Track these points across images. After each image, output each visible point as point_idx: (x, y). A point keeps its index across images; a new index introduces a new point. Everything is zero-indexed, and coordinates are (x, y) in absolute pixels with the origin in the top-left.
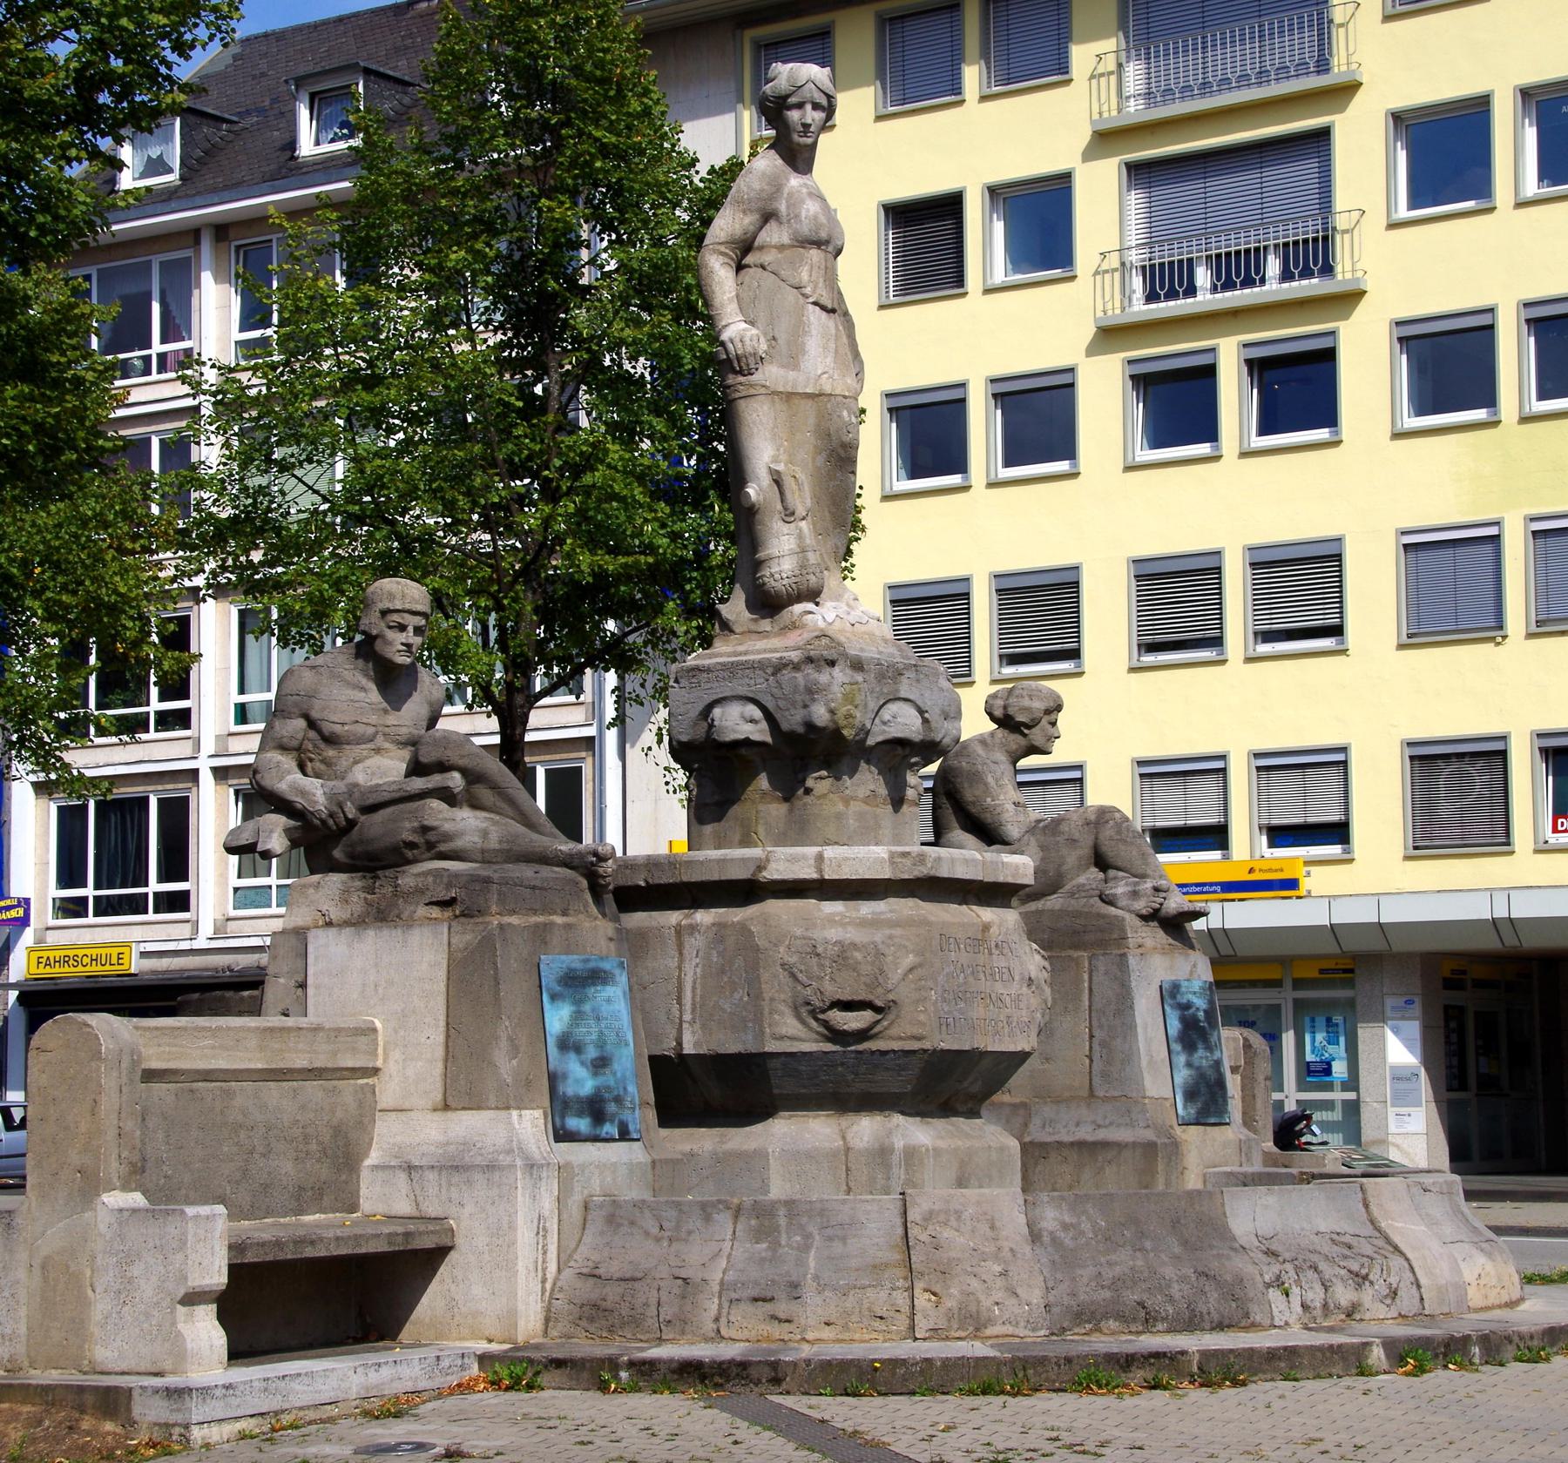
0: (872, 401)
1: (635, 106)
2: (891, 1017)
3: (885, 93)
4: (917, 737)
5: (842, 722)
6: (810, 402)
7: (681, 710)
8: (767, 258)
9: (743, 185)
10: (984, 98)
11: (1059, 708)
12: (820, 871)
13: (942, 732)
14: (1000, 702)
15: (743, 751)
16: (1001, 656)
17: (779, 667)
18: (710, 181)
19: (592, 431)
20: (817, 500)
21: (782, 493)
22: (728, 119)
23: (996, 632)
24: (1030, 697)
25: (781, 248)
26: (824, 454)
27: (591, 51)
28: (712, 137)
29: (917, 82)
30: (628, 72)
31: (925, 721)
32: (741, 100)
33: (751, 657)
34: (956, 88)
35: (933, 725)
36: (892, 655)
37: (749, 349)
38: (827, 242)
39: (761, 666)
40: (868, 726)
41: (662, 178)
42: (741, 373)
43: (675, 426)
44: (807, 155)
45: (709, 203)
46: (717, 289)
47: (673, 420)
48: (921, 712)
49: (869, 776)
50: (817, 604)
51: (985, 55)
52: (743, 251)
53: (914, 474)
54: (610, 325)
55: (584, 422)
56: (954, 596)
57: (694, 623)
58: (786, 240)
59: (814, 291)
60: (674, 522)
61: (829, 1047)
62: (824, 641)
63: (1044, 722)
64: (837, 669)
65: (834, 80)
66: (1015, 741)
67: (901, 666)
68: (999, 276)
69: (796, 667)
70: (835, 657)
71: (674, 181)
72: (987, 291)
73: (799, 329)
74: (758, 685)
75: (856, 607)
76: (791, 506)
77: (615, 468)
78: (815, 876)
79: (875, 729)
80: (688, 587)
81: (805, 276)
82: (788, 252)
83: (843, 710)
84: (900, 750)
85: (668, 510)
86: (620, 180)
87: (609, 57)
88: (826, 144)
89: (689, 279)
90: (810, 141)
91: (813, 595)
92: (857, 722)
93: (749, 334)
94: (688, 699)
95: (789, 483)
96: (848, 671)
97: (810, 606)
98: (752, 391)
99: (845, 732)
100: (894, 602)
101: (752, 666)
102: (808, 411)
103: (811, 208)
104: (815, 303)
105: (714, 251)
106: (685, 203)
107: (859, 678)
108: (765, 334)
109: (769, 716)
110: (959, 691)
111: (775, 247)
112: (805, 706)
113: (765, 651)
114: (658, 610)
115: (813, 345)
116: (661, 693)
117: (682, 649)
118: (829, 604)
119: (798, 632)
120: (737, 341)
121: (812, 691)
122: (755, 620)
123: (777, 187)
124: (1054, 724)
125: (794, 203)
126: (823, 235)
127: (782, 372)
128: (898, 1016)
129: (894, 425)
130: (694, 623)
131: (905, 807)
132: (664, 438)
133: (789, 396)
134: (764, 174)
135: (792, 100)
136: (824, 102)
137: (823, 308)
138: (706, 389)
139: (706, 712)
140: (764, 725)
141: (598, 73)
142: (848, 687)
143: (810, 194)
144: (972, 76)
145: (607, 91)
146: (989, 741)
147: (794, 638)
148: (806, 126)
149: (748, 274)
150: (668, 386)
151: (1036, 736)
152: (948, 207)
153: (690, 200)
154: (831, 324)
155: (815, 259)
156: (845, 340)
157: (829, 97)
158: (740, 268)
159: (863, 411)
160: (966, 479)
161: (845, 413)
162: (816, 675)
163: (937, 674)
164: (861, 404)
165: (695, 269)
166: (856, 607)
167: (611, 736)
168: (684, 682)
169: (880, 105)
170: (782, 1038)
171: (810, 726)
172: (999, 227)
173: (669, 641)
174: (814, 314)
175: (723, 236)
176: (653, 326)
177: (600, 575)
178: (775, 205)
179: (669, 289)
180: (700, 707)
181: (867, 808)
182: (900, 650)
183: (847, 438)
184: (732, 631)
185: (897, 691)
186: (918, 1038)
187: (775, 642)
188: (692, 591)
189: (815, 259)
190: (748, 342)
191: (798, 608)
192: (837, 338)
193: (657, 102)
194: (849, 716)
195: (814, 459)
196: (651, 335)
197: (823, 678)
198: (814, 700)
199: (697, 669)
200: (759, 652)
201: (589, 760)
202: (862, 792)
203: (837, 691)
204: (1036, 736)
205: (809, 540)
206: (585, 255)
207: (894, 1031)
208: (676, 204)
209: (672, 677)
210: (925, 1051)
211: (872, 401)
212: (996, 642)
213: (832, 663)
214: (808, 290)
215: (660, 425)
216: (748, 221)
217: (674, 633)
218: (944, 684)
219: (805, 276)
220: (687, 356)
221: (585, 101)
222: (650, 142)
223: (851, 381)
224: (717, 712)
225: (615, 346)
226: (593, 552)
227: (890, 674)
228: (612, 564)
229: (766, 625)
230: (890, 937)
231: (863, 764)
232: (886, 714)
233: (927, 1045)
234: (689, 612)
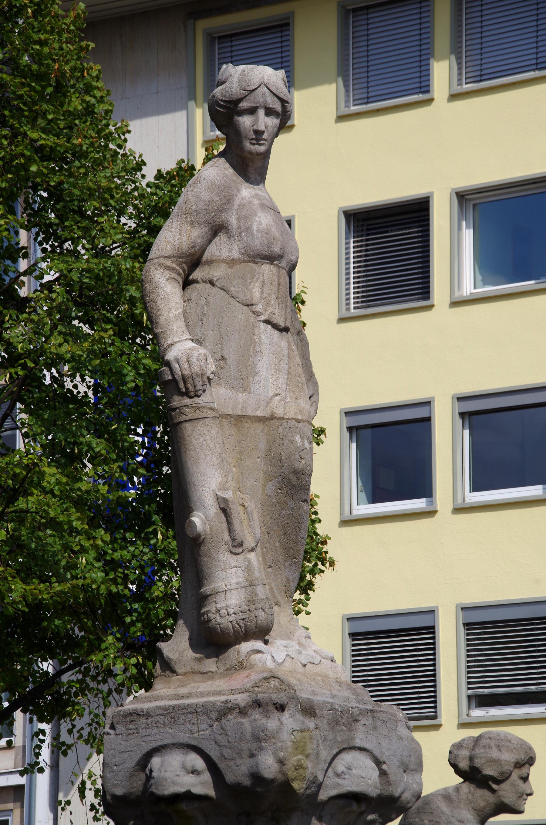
0: (329, 417)
1: (76, 104)
3: (347, 91)
4: (373, 792)
5: (292, 774)
6: (260, 427)
7: (118, 759)
8: (217, 272)
9: (192, 195)
10: (454, 97)
11: (531, 761)
13: (402, 785)
14: (465, 753)
15: (183, 806)
16: (469, 697)
17: (225, 711)
18: (157, 186)
19: (28, 453)
20: (267, 530)
21: (229, 523)
22: (180, 116)
23: (464, 670)
24: (499, 748)
25: (231, 262)
26: (275, 482)
27: (28, 41)
28: (162, 137)
29: (383, 79)
30: (67, 68)
31: (383, 774)
32: (192, 96)
33: (194, 701)
34: (424, 87)
35: (392, 777)
36: (348, 699)
37: (196, 369)
38: (280, 257)
39: (204, 710)
40: (320, 778)
41: (104, 183)
42: (187, 394)
43: (116, 447)
44: (259, 164)
45: (156, 212)
46: (162, 305)
47: (113, 440)
48: (378, 763)
50: (266, 642)
51: (456, 50)
52: (191, 264)
53: (374, 499)
54: (47, 338)
55: (20, 444)
56: (419, 632)
57: (133, 661)
58: (236, 255)
59: (266, 309)
60: (114, 550)
62: (273, 683)
63: (515, 776)
64: (287, 714)
65: (290, 83)
66: (483, 797)
67: (356, 711)
68: (468, 288)
69: (243, 712)
70: (284, 700)
71: (117, 188)
72: (455, 304)
73: (250, 348)
74: (202, 732)
75: (311, 645)
76: (239, 537)
77: (52, 492)
79: (328, 782)
80: (128, 620)
81: (256, 292)
82: (238, 267)
83: (293, 761)
84: (355, 806)
85: (108, 538)
86: (61, 183)
87: (46, 50)
88: (282, 150)
89: (133, 291)
90: (262, 149)
91: (262, 633)
92: (308, 774)
93: (196, 354)
94: (125, 747)
95: (236, 511)
96: (299, 717)
97: (258, 644)
98: (199, 414)
99: (295, 785)
100: (353, 635)
101: (195, 711)
102: (258, 435)
103: (263, 220)
104: (267, 322)
105: (160, 265)
106: (130, 209)
107: (311, 724)
108: (213, 354)
109: (212, 766)
110: (418, 736)
111: (225, 262)
112: (252, 756)
113: (209, 694)
114: (95, 646)
115: (264, 365)
116: (95, 741)
117: (119, 692)
118: (279, 643)
119: (245, 673)
120: (183, 360)
121: (259, 739)
122: (199, 660)
123: (227, 198)
124: (525, 779)
125: (245, 216)
126: (276, 249)
127: (231, 393)
129: (354, 445)
130: (133, 661)
132: (106, 461)
133: (238, 420)
134: (213, 184)
135: (244, 105)
136: (278, 107)
137: (275, 326)
138: (153, 402)
139: (144, 762)
140: (207, 777)
141: (35, 67)
142: (298, 735)
143: (263, 206)
144: (442, 72)
145: (44, 88)
146: (454, 796)
147: (241, 680)
148: (259, 133)
149: (195, 290)
150: (111, 404)
151: (506, 792)
152: (413, 214)
153: (135, 207)
154: (284, 343)
155: (267, 275)
156: (298, 359)
157: (283, 102)
158: (187, 283)
159: (322, 431)
160: (432, 503)
161: (298, 438)
162: (264, 721)
163: (395, 721)
164: (317, 423)
165: (140, 283)
166: (311, 645)
167: (42, 781)
168: (120, 728)
169: (343, 104)
171: (257, 778)
172: (468, 236)
173: (105, 681)
174: (266, 334)
175: (169, 250)
176: (94, 342)
177: (37, 606)
178: (225, 217)
179: (111, 302)
180: (137, 756)
182: (356, 694)
183: (300, 465)
184: (174, 672)
185: (353, 739)
187: (221, 684)
188: (133, 623)
189: (267, 275)
190: (195, 362)
191: (246, 647)
192: (290, 358)
193: (101, 100)
194: (299, 767)
195: (264, 487)
196: (91, 352)
197: (272, 724)
198: (261, 749)
199: (135, 714)
200: (203, 695)
201: (17, 812)
203: (286, 739)
204: (506, 792)
205: (258, 573)
206: (23, 265)
208: (121, 212)
209: (108, 722)
211: (329, 417)
212: (464, 681)
213: (281, 708)
214: (259, 308)
215: (99, 446)
216: (197, 234)
217: (110, 673)
218: (403, 731)
219: (256, 292)
220: (130, 375)
221: (21, 97)
222: (92, 145)
223: (304, 403)
224: (156, 761)
225: (55, 361)
226: (25, 581)
227: (344, 720)
228: (43, 592)
229: (211, 665)
232: (340, 765)
234: (130, 647)
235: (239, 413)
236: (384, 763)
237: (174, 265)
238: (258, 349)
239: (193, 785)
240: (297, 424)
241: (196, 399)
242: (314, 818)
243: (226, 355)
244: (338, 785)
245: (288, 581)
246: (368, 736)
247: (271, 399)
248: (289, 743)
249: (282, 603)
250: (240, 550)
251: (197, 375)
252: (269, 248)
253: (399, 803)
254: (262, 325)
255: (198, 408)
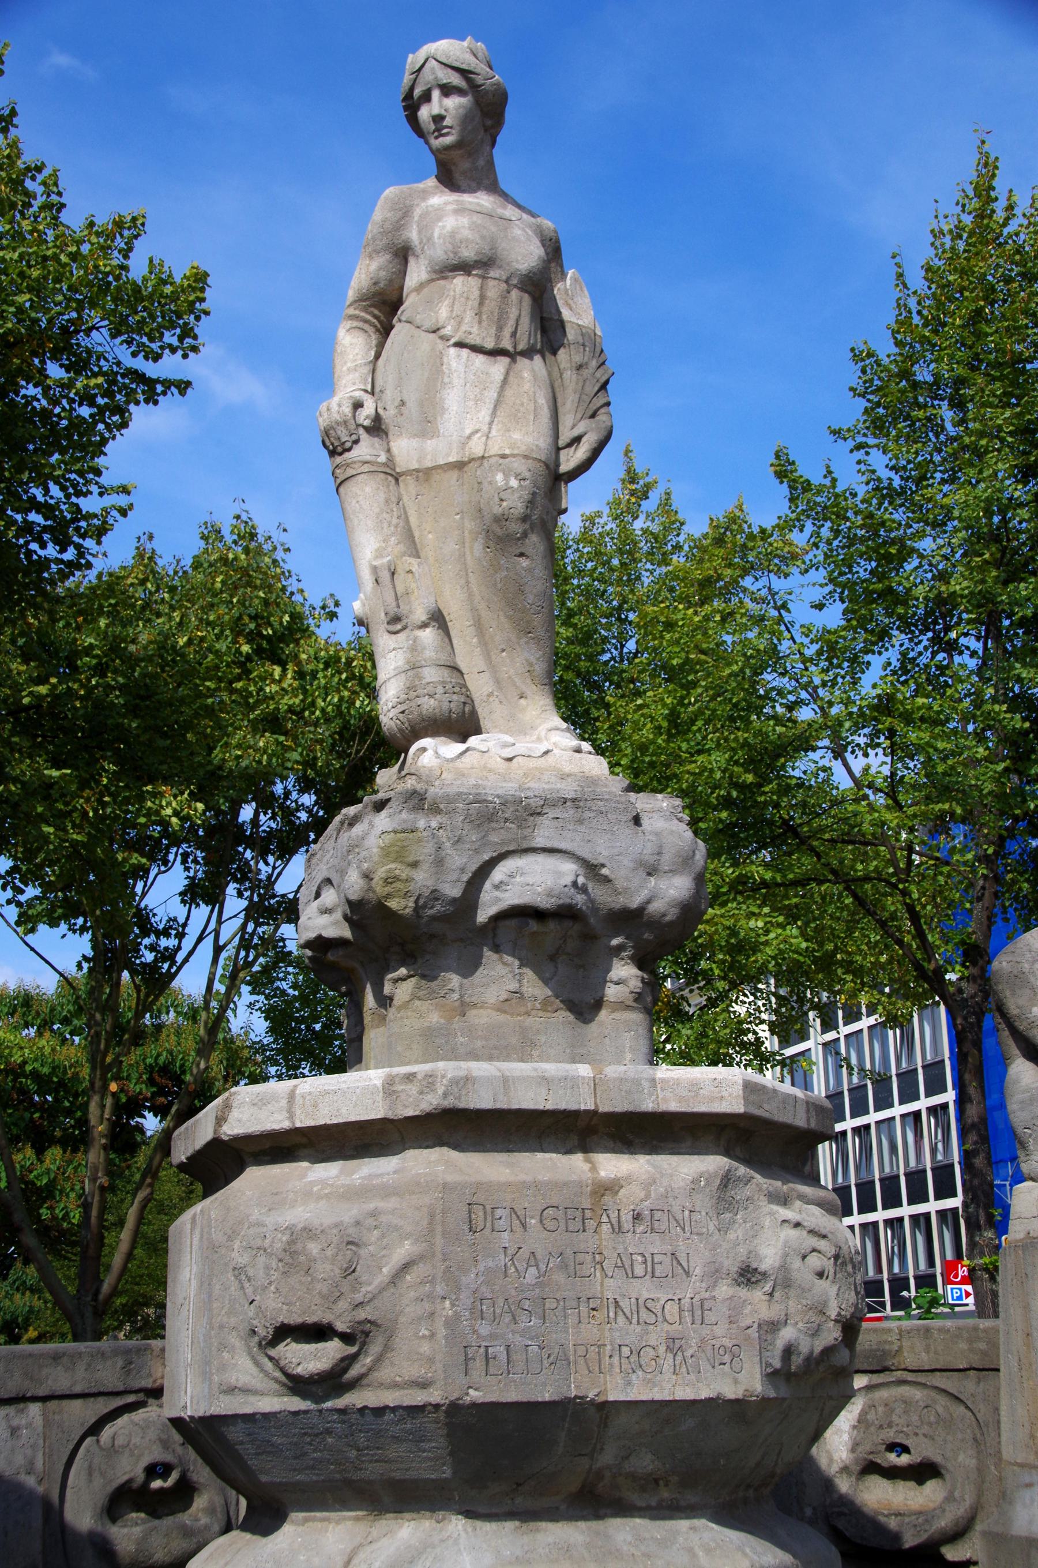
2: (374, 1349)
6: (454, 474)
12: (291, 1117)
49: (500, 970)
59: (456, 330)
61: (296, 1404)
78: (286, 1125)
98: (350, 472)
99: (393, 904)
104: (460, 345)
127: (415, 443)
128: (387, 1348)
131: (603, 1014)
170: (231, 1390)
181: (502, 1018)
186: (424, 1385)
202: (494, 994)
207: (385, 1373)
210: (437, 1406)
214: (448, 331)
230: (374, 1214)
231: (488, 954)
233: (434, 1396)
235: (429, 464)
236: (603, 866)
237: (357, 312)
238: (446, 380)
239: (325, 927)
240: (501, 461)
241: (347, 455)
242: (485, 949)
243: (405, 399)
244: (498, 900)
245: (531, 665)
246: (565, 833)
247: (469, 437)
248: (375, 850)
249: (528, 693)
250: (399, 627)
251: (338, 423)
252: (455, 253)
253: (645, 918)
254: (453, 351)
255: (348, 465)
